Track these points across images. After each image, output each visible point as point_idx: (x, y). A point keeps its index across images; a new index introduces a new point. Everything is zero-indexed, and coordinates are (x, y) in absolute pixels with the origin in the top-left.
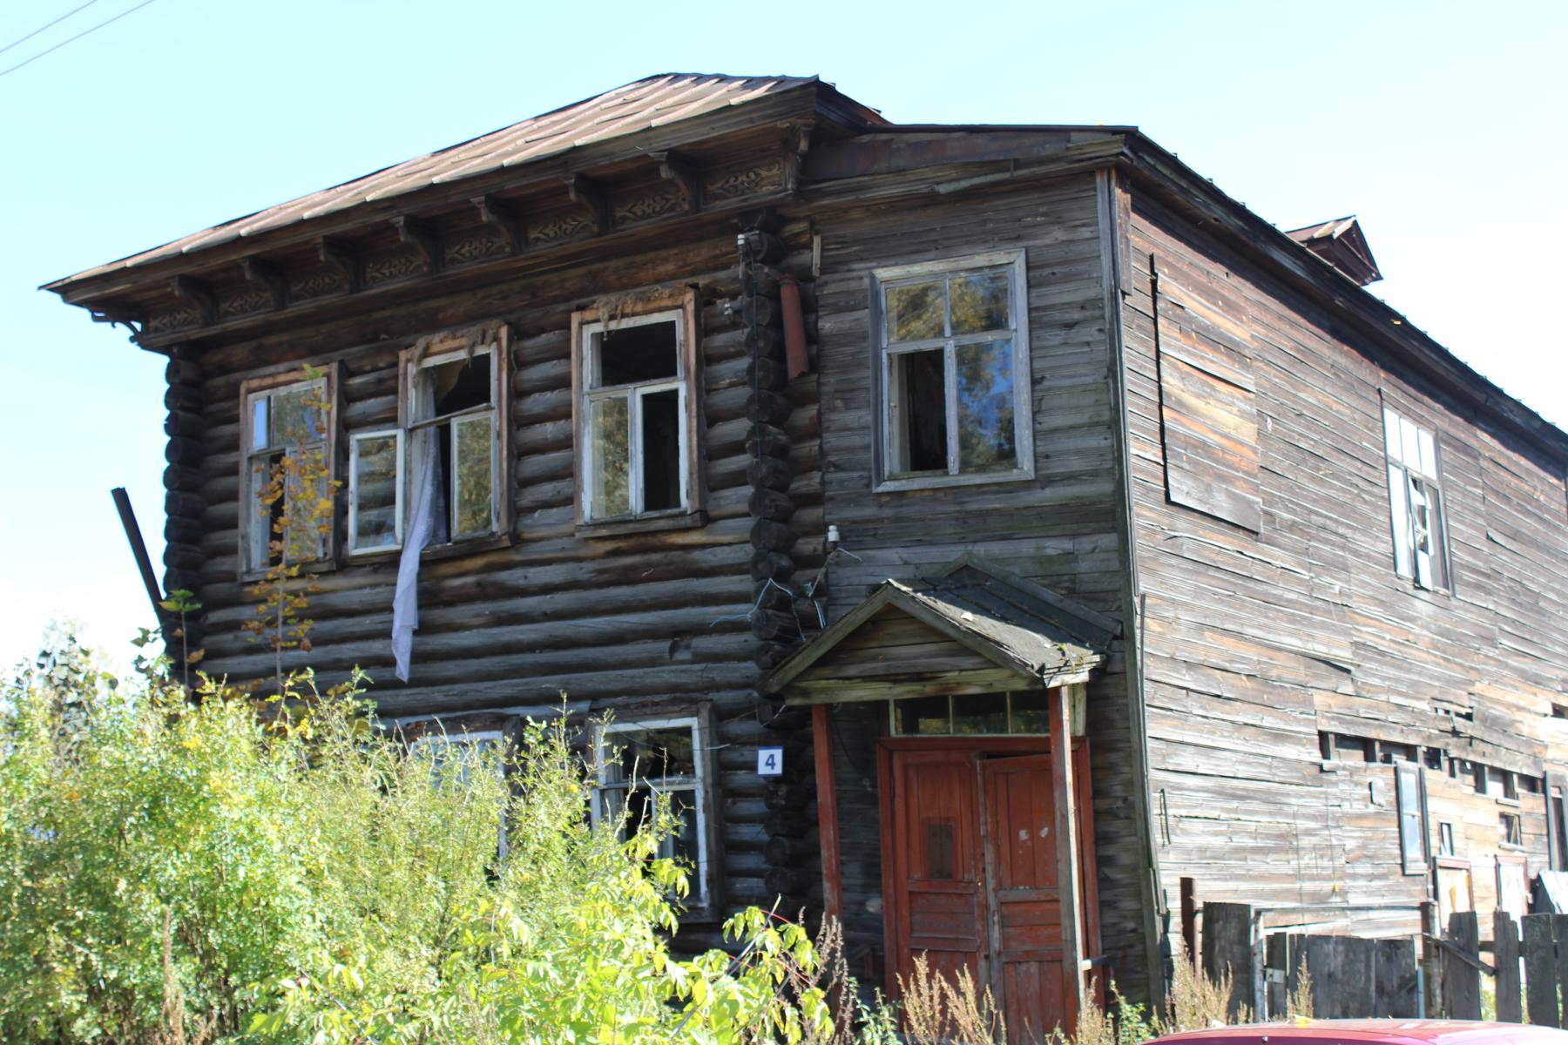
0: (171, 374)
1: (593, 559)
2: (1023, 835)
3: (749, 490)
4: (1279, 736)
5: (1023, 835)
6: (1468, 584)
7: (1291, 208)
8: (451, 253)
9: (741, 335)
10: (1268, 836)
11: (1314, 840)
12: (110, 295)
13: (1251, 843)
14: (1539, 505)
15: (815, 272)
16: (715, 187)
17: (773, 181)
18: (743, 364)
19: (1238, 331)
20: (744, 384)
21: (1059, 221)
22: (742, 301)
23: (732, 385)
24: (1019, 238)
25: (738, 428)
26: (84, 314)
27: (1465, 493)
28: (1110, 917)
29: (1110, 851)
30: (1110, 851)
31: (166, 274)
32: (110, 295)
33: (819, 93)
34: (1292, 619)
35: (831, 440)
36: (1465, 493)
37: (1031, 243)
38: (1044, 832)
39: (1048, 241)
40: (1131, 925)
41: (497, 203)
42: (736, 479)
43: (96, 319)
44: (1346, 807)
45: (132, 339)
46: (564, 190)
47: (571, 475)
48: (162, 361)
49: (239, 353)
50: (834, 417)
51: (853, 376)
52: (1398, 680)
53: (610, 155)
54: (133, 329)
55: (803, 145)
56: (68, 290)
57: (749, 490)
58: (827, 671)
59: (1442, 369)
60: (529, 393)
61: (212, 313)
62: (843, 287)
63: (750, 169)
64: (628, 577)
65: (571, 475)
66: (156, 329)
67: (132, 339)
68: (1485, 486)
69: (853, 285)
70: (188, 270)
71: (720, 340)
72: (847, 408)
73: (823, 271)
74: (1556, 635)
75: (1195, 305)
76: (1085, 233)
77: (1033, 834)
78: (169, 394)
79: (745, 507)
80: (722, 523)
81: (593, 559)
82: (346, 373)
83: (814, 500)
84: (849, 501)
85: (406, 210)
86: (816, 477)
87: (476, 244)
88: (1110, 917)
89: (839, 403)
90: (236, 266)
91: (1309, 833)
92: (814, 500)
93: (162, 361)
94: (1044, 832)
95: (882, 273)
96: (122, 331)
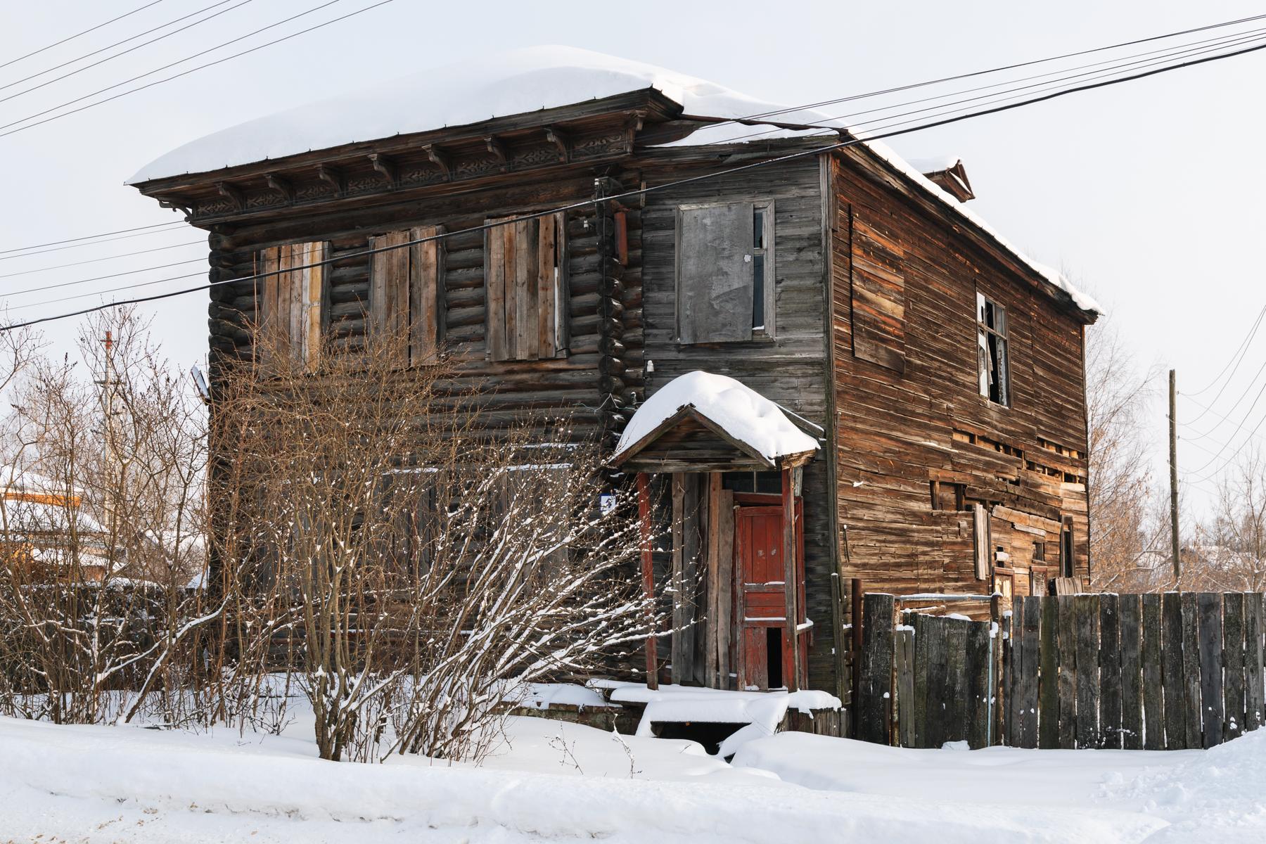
0: (213, 242)
1: (495, 375)
2: (761, 553)
3: (598, 337)
4: (910, 497)
5: (761, 553)
6: (1021, 401)
7: (1169, 466)
8: (406, 178)
9: (595, 240)
10: (900, 556)
11: (927, 558)
12: (171, 191)
13: (893, 560)
14: (1066, 350)
15: (642, 204)
16: (581, 147)
17: (619, 146)
18: (594, 259)
19: (898, 250)
20: (595, 271)
21: (797, 184)
22: (595, 218)
23: (587, 272)
24: (771, 192)
25: (591, 298)
26: (155, 202)
27: (1021, 343)
28: (812, 604)
29: (812, 564)
30: (812, 564)
31: (214, 180)
32: (171, 191)
33: (652, 95)
34: (920, 425)
35: (651, 308)
36: (1021, 343)
37: (779, 196)
38: (773, 552)
39: (788, 195)
40: (823, 608)
41: (441, 150)
42: (591, 330)
43: (162, 206)
44: (945, 538)
45: (186, 220)
46: (485, 143)
47: (366, 280)
48: (206, 234)
49: (259, 231)
50: (651, 295)
51: (663, 270)
52: (978, 461)
53: (515, 125)
54: (187, 212)
55: (639, 126)
56: (146, 187)
57: (598, 337)
58: (652, 453)
59: (1013, 267)
60: (456, 269)
61: (244, 210)
62: (658, 214)
63: (603, 137)
64: (520, 387)
65: (366, 280)
66: (203, 213)
67: (186, 220)
68: (1033, 339)
69: (666, 214)
70: (228, 178)
71: (580, 242)
72: (660, 290)
73: (647, 203)
74: (1071, 431)
75: (872, 236)
76: (811, 192)
77: (767, 553)
78: (211, 255)
79: (595, 347)
80: (578, 357)
81: (495, 375)
82: (334, 249)
83: (637, 345)
84: (662, 347)
85: (379, 150)
86: (640, 331)
87: (422, 173)
88: (812, 604)
89: (655, 287)
90: (261, 177)
91: (924, 553)
92: (637, 345)
93: (206, 234)
94: (773, 552)
95: (683, 207)
96: (180, 214)
